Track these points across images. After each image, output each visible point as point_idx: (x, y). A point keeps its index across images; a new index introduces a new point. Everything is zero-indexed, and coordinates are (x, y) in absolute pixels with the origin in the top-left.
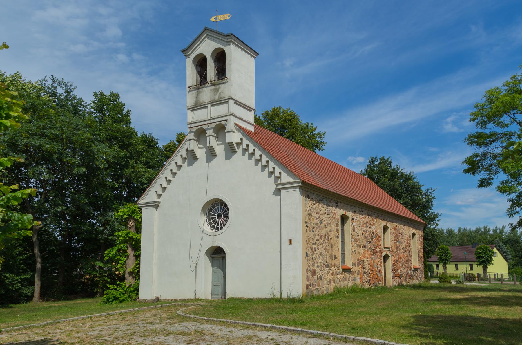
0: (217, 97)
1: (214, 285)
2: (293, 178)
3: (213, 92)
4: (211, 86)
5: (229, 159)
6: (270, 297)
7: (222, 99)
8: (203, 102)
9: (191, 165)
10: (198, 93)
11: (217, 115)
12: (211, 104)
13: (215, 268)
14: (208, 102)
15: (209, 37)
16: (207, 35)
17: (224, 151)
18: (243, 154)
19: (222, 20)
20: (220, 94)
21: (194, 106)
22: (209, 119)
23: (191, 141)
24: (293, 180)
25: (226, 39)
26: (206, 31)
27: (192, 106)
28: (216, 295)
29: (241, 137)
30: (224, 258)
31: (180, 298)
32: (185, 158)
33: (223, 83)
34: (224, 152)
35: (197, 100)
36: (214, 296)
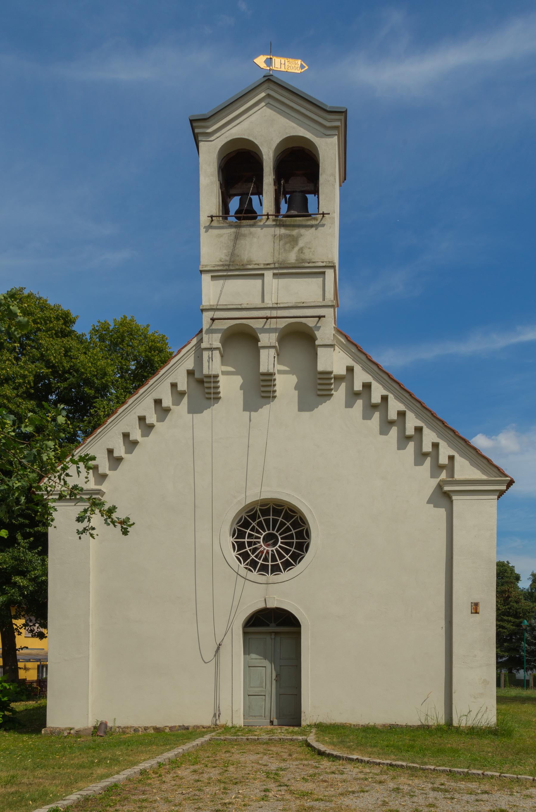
0: (292, 257)
1: (248, 695)
2: (484, 472)
3: (282, 243)
4: (276, 226)
5: (311, 410)
6: (420, 724)
7: (307, 265)
8: (250, 262)
9: (200, 411)
10: (237, 237)
11: (291, 300)
12: (275, 271)
13: (253, 656)
14: (268, 264)
15: (272, 102)
16: (268, 96)
17: (296, 388)
18: (349, 404)
19: (283, 69)
20: (301, 250)
21: (225, 268)
22: (271, 306)
23: (214, 352)
24: (484, 477)
25: (326, 120)
26: (266, 85)
27: (218, 266)
28: (255, 716)
29: (350, 362)
30: (298, 635)
31: (170, 725)
32: (182, 394)
33: (312, 226)
34: (297, 392)
35: (233, 254)
36: (251, 721)
